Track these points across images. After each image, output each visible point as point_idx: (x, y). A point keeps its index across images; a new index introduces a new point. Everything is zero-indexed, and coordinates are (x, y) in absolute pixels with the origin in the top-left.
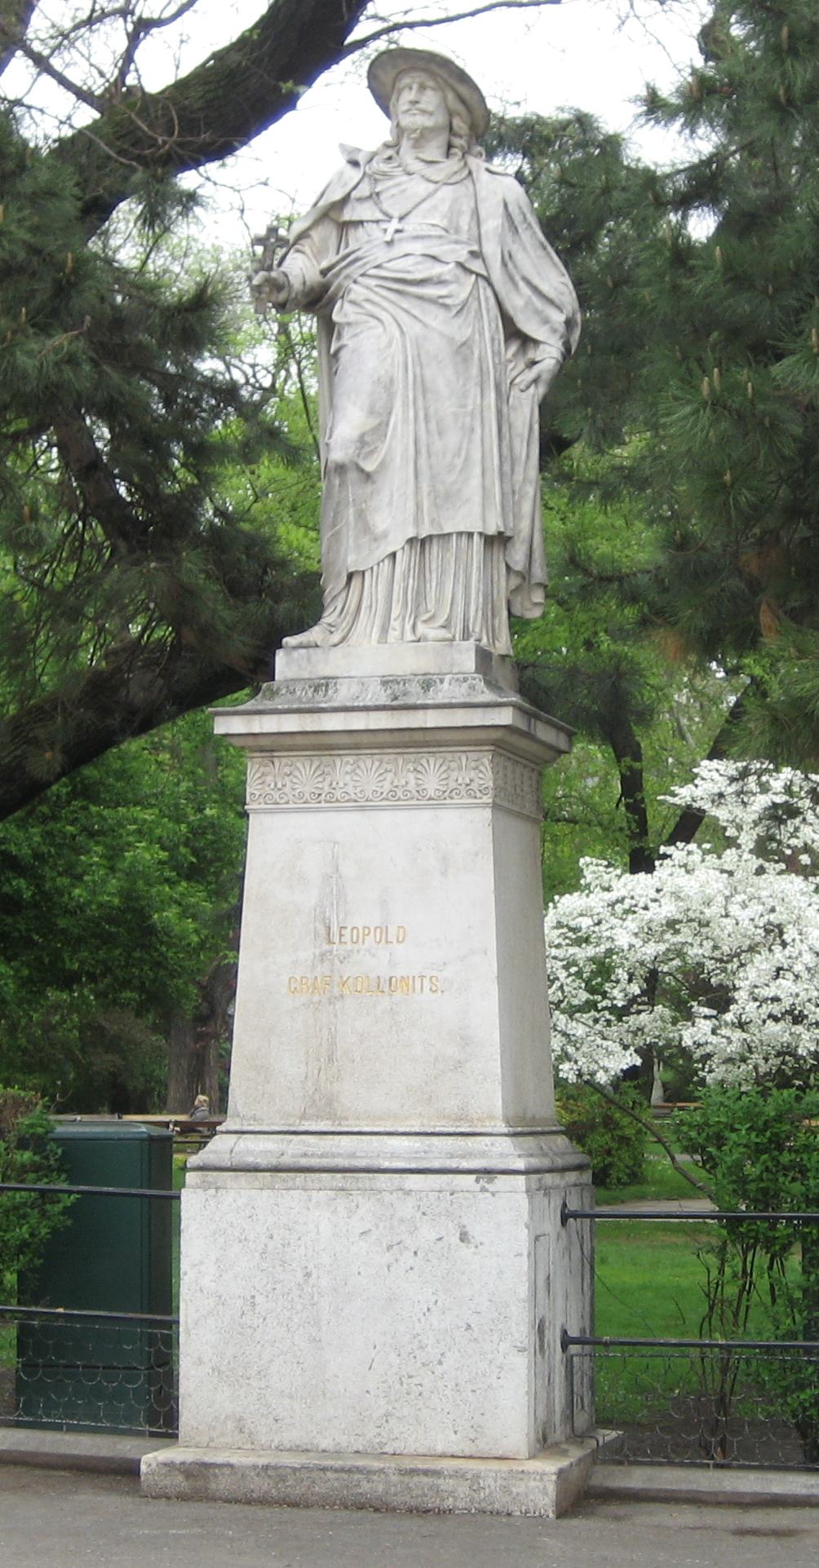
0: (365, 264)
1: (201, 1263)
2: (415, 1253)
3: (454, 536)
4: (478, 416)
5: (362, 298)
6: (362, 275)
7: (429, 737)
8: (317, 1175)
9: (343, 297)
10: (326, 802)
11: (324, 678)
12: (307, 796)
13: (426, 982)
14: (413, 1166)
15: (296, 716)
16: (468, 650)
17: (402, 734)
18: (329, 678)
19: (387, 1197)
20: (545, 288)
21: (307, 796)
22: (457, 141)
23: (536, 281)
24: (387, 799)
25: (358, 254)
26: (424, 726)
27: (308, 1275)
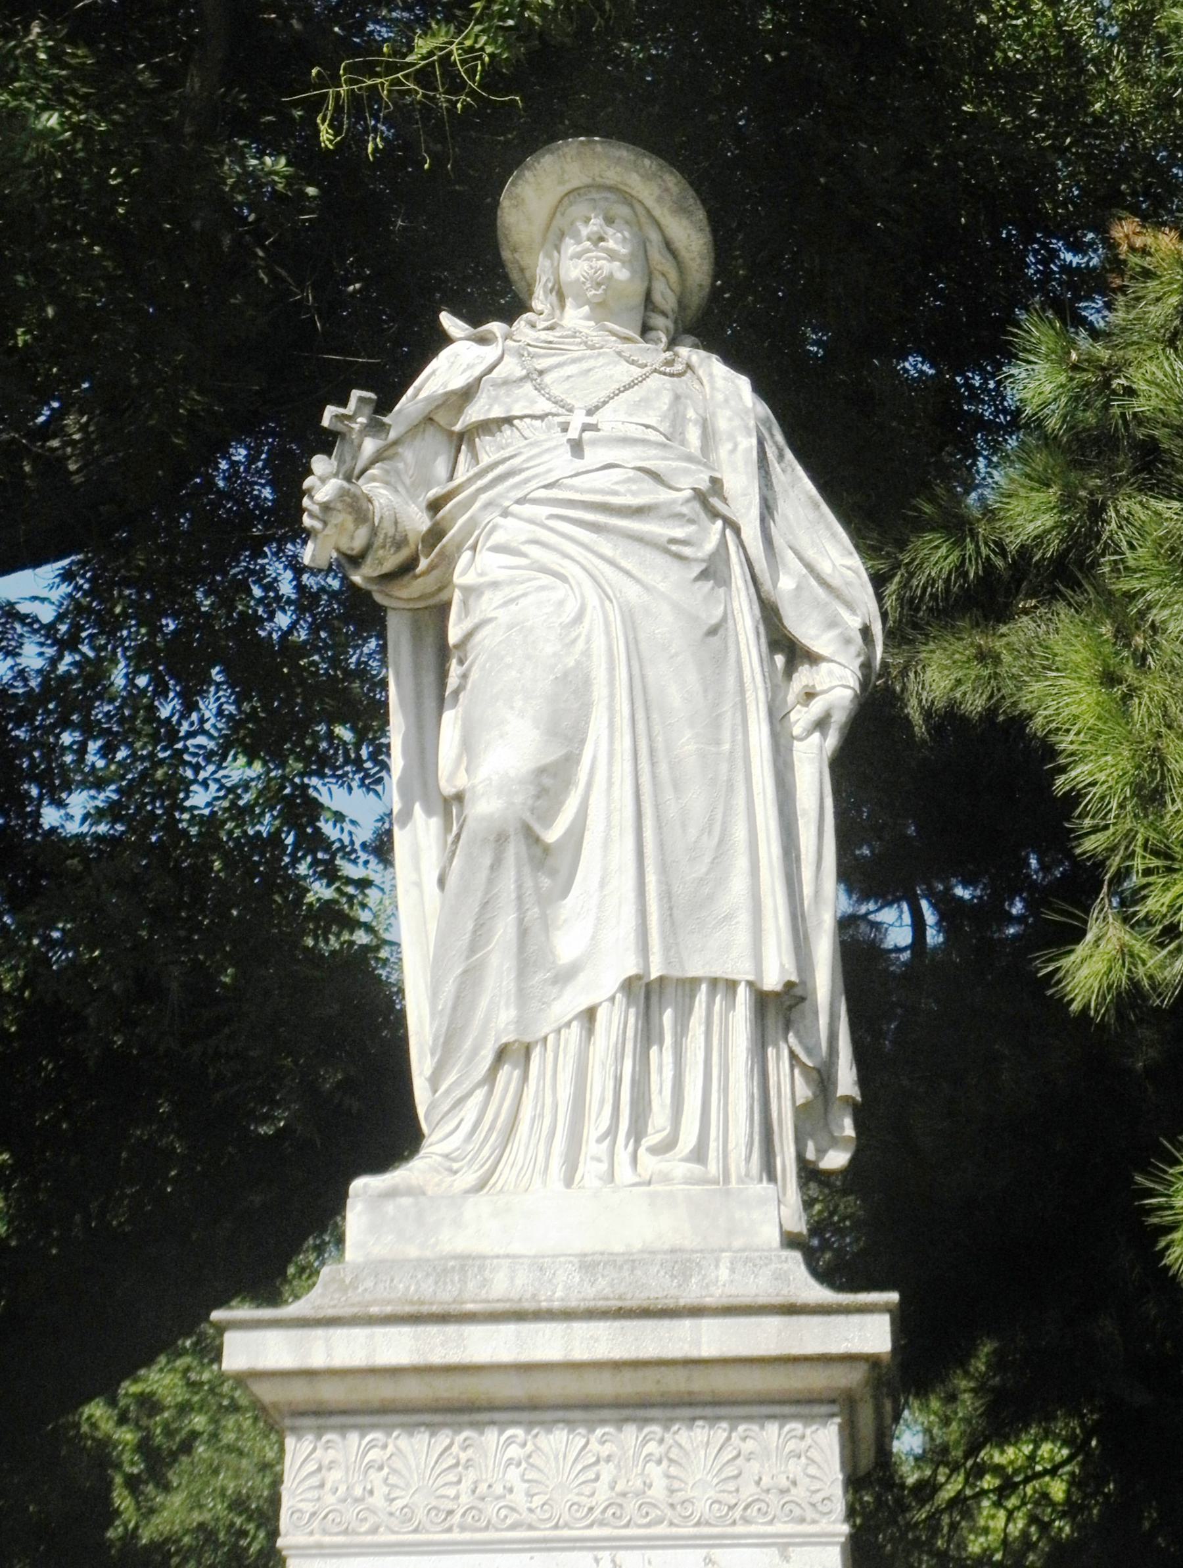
0: (527, 481)
3: (704, 987)
4: (740, 764)
5: (523, 538)
6: (519, 502)
7: (701, 1383)
9: (474, 548)
10: (463, 1528)
12: (420, 1514)
15: (406, 1331)
17: (640, 1373)
18: (469, 1257)
20: (825, 568)
21: (420, 1514)
22: (658, 321)
23: (811, 554)
24: (602, 1523)
25: (515, 462)
26: (694, 1353)
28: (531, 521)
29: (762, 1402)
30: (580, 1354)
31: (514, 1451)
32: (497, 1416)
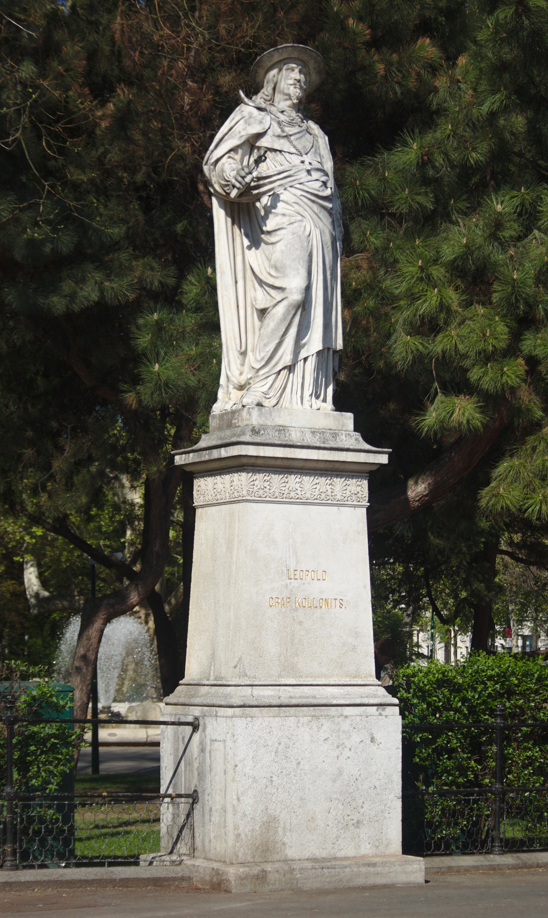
0: (294, 180)
1: (245, 759)
2: (350, 749)
5: (293, 201)
6: (291, 187)
8: (301, 708)
11: (282, 426)
12: (277, 494)
13: (337, 601)
14: (348, 702)
16: (350, 418)
19: (337, 720)
26: (346, 460)
27: (299, 763)
28: (295, 195)
29: (321, 470)
30: (321, 458)
31: (358, 483)
32: (294, 470)
